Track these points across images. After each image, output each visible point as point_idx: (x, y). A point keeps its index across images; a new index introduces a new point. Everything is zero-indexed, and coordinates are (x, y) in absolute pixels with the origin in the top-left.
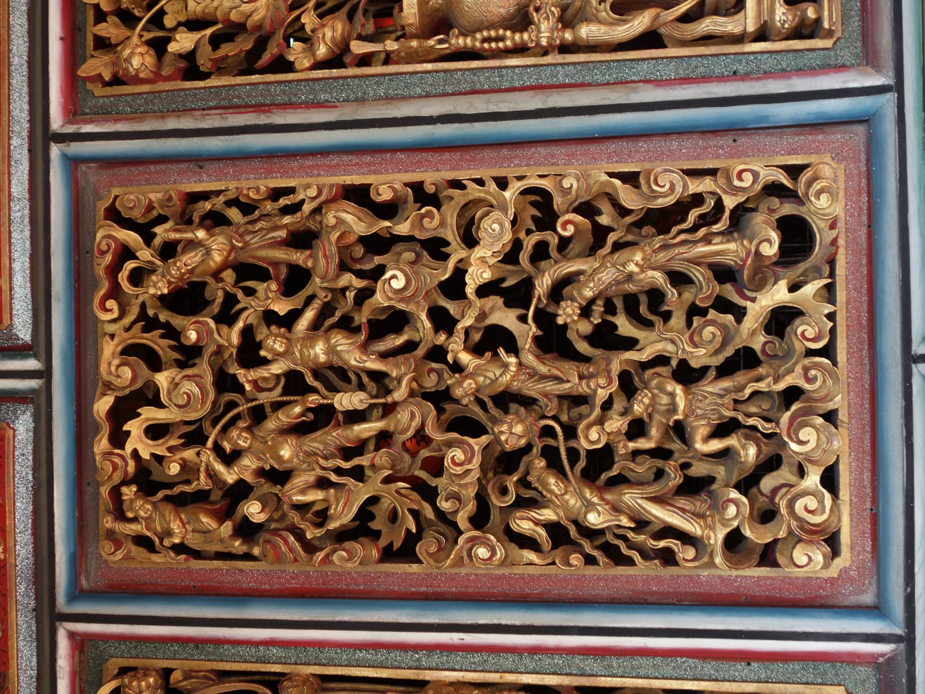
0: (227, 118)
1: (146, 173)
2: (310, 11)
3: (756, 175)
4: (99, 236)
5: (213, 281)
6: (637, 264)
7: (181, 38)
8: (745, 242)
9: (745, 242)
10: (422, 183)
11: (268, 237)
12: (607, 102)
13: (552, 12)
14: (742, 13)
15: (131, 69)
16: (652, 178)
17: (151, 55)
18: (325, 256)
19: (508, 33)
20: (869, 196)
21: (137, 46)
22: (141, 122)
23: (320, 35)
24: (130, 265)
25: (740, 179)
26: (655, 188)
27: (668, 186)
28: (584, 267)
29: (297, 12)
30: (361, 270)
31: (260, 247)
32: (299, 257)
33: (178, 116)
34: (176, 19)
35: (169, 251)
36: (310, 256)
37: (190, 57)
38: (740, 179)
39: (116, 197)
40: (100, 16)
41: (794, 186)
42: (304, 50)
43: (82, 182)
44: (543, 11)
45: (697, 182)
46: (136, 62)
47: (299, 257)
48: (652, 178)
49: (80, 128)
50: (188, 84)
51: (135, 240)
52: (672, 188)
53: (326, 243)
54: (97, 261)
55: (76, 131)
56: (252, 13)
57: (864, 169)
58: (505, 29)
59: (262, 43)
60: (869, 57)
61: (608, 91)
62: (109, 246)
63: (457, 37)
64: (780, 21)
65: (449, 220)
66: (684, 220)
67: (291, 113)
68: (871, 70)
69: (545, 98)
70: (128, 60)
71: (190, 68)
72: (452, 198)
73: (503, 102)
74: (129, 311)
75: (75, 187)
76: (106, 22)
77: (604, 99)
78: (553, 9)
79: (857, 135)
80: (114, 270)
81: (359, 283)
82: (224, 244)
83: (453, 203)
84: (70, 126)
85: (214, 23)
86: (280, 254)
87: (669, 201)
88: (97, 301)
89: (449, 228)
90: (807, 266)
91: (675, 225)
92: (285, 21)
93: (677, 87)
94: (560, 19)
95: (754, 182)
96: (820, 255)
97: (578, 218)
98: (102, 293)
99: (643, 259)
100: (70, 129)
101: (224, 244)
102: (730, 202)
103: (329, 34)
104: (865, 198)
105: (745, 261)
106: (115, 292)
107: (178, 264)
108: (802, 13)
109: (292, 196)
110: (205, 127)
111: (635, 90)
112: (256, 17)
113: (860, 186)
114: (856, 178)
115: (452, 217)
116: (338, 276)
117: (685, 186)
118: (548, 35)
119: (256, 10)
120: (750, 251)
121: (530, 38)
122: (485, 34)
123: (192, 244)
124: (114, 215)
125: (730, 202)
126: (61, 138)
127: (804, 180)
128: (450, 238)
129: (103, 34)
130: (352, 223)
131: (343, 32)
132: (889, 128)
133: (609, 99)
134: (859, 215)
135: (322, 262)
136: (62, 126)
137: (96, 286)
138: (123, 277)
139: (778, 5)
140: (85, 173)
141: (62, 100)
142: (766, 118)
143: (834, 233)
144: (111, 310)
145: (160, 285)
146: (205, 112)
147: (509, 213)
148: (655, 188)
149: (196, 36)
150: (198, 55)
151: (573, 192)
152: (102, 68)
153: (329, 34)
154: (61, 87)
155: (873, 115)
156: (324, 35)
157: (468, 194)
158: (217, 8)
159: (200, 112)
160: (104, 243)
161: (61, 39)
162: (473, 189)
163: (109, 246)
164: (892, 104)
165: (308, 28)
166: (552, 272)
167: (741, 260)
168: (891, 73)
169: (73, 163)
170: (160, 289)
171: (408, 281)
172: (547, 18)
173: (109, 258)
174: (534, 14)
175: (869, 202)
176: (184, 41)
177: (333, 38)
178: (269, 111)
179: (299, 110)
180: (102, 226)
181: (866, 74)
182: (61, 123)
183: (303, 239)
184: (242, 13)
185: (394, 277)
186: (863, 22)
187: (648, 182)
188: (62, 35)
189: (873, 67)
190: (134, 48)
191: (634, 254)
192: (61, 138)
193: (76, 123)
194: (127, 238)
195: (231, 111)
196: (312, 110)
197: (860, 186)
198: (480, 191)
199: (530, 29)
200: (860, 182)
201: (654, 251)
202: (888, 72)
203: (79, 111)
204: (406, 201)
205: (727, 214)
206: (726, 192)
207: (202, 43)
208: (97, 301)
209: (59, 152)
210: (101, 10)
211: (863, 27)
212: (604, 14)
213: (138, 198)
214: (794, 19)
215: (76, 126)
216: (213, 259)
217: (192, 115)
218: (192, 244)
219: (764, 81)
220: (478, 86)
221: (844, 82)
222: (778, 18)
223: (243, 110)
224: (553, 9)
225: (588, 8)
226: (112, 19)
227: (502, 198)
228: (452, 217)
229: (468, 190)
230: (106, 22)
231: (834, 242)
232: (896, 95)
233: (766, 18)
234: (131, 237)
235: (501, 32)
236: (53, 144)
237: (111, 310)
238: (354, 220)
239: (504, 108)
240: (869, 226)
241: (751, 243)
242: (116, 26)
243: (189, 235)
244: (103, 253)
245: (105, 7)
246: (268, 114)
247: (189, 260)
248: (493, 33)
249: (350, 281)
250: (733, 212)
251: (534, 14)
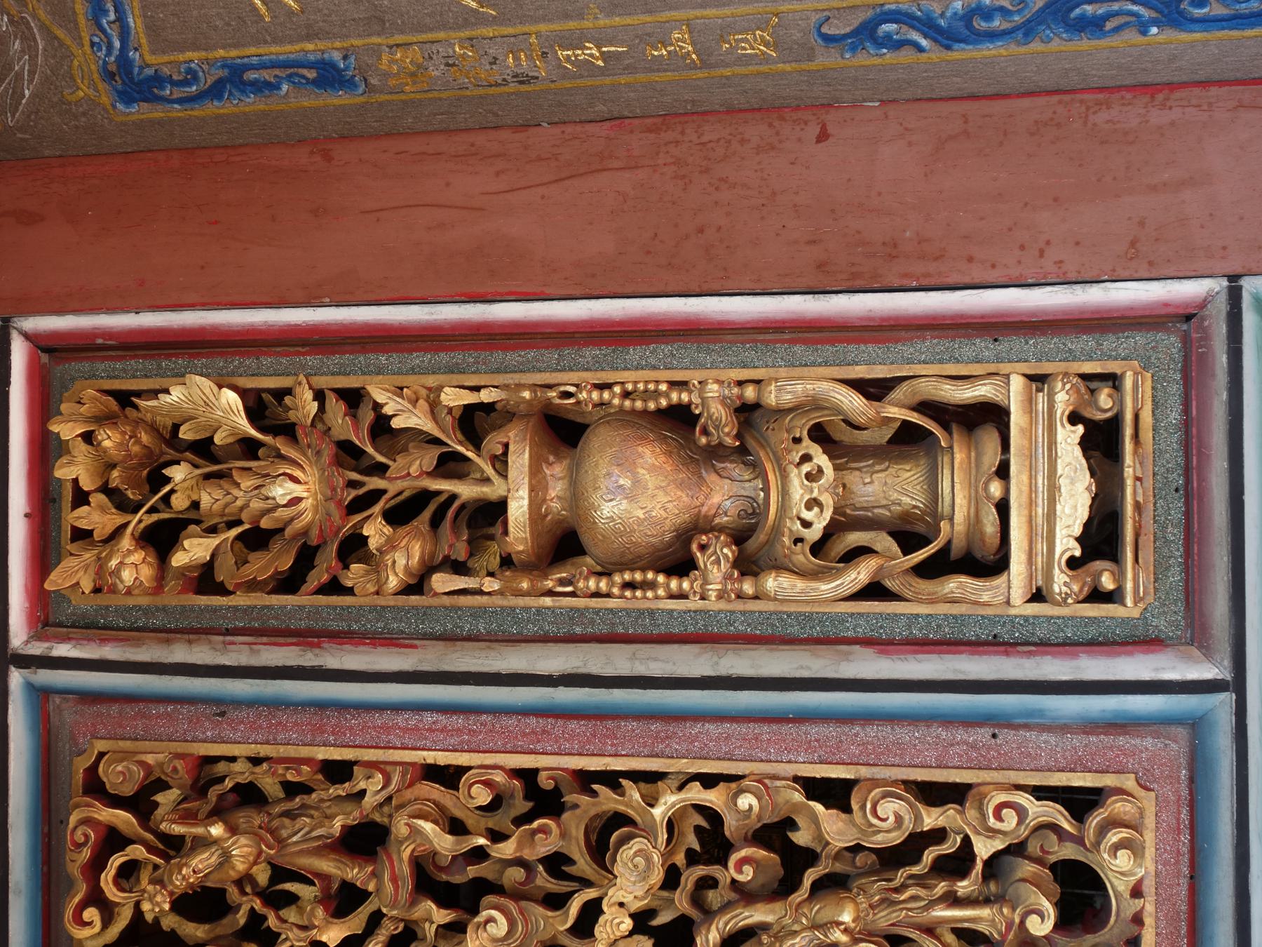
0: (259, 651)
1: (144, 716)
2: (377, 517)
3: (1021, 812)
4: (73, 819)
5: (236, 891)
6: (846, 931)
7: (191, 545)
8: (1005, 910)
9: (1005, 910)
10: (534, 772)
11: (314, 834)
12: (806, 674)
13: (726, 556)
14: (1004, 577)
15: (121, 586)
16: (869, 806)
17: (149, 563)
18: (394, 879)
19: (661, 578)
20: (1192, 834)
21: (129, 552)
22: (138, 646)
23: (389, 563)
24: (116, 861)
25: (999, 817)
26: (874, 821)
27: (892, 819)
28: (770, 918)
29: (357, 518)
30: (448, 883)
31: (301, 852)
32: (355, 873)
33: (190, 642)
34: (189, 497)
35: (173, 847)
36: (373, 874)
37: (208, 568)
38: (999, 817)
39: (101, 755)
40: (81, 498)
41: (1080, 831)
42: (367, 573)
43: (54, 720)
44: (711, 549)
45: (936, 811)
46: (127, 576)
47: (355, 873)
48: (869, 806)
49: (51, 648)
50: (204, 600)
51: (128, 822)
52: (899, 819)
53: (395, 857)
54: (69, 856)
55: (46, 653)
56: (292, 519)
57: (1185, 792)
58: (658, 571)
59: (306, 557)
60: (1195, 636)
61: (808, 653)
62: (87, 836)
63: (587, 579)
64: (1060, 594)
65: (574, 832)
66: (917, 860)
67: (350, 652)
68: (1197, 653)
69: (715, 659)
70: (116, 572)
71: (205, 579)
72: (576, 806)
73: (656, 659)
74: (119, 914)
75: (45, 727)
76: (88, 504)
77: (802, 667)
78: (725, 551)
79: (1176, 742)
80: (96, 866)
81: (442, 916)
82: (246, 846)
83: (578, 811)
84: (38, 644)
85: (239, 522)
86: (326, 865)
87: (896, 838)
88: (69, 913)
89: (573, 842)
90: (1097, 940)
91: (904, 865)
92: (339, 530)
93: (910, 657)
94: (736, 564)
95: (1019, 824)
96: (1116, 931)
97: (761, 853)
98: (77, 900)
99: (854, 921)
100: (37, 649)
101: (246, 846)
102: (983, 849)
103: (401, 562)
104: (1185, 838)
105: (1004, 936)
106: (96, 898)
107: (184, 872)
108: (1093, 580)
109: (347, 785)
110: (228, 663)
111: (847, 657)
112: (298, 525)
113: (1178, 820)
114: (1173, 808)
115: (577, 827)
116: (413, 903)
117: (918, 818)
118: (719, 587)
119: (300, 514)
120: (1013, 922)
121: (692, 587)
122: (627, 576)
123: (204, 843)
124: (95, 788)
125: (983, 849)
126: (26, 662)
127: (1094, 824)
128: (576, 856)
129: (83, 524)
130: (431, 836)
131: (423, 553)
132: (1223, 742)
133: (809, 668)
134: (1177, 862)
135: (389, 887)
136: (27, 642)
137: (70, 884)
138: (107, 879)
139: (1057, 571)
140: (59, 707)
141: (27, 605)
142: (1040, 713)
143: (1139, 903)
144: (89, 924)
145: (159, 898)
146: (229, 638)
147: (660, 840)
148: (874, 821)
149: (213, 542)
150: (216, 564)
151: (753, 816)
152: (81, 573)
153: (401, 562)
154: (26, 585)
155: (1201, 718)
156: (394, 562)
157: (600, 803)
158: (242, 509)
159: (221, 638)
160: (79, 832)
161: (26, 515)
162: (607, 799)
163: (87, 836)
164: (1227, 708)
165: (373, 544)
166: (721, 925)
167: (1000, 933)
168: (1227, 662)
169: (41, 696)
170: (158, 904)
171: (512, 923)
172: (718, 562)
173: (86, 853)
174: (698, 554)
175: (1192, 841)
176: (195, 550)
177: (407, 566)
178: (318, 646)
179: (361, 648)
180: (77, 806)
181: (1189, 658)
182: (25, 638)
183: (366, 840)
184: (277, 520)
185: (491, 920)
186: (1187, 573)
187: (863, 807)
188: (28, 510)
189: (1200, 648)
190: (124, 556)
191: (842, 911)
192: (26, 662)
193: (46, 638)
194: (114, 820)
195: (265, 639)
196: (380, 649)
197: (1178, 820)
198: (616, 801)
199: (691, 574)
200: (1179, 813)
201: (872, 907)
202: (1222, 659)
203: (51, 620)
204: (512, 796)
205: (979, 866)
206: (978, 833)
207: (222, 550)
208: (69, 913)
209: (21, 680)
210: (80, 489)
211: (1187, 581)
212: (801, 558)
213: (129, 769)
214: (1081, 590)
215: (46, 645)
216: (233, 868)
217: (210, 642)
218: (204, 843)
219: (1038, 658)
220: (620, 630)
221: (1157, 670)
222: (1057, 590)
223: (281, 640)
224: (725, 551)
225: (778, 547)
226: (98, 499)
227: (649, 817)
228: (577, 827)
229: (601, 798)
230: (88, 504)
231: (1138, 920)
232: (1234, 697)
233: (1040, 583)
234: (123, 818)
235: (650, 575)
236: (12, 668)
237: (89, 924)
238: (434, 831)
239: (656, 669)
240: (1192, 877)
241: (1014, 910)
242: (103, 509)
243: (199, 830)
244: (79, 846)
245: (86, 485)
246: (317, 651)
247: (199, 865)
248: (638, 576)
249: (429, 912)
250: (988, 863)
251: (698, 554)
